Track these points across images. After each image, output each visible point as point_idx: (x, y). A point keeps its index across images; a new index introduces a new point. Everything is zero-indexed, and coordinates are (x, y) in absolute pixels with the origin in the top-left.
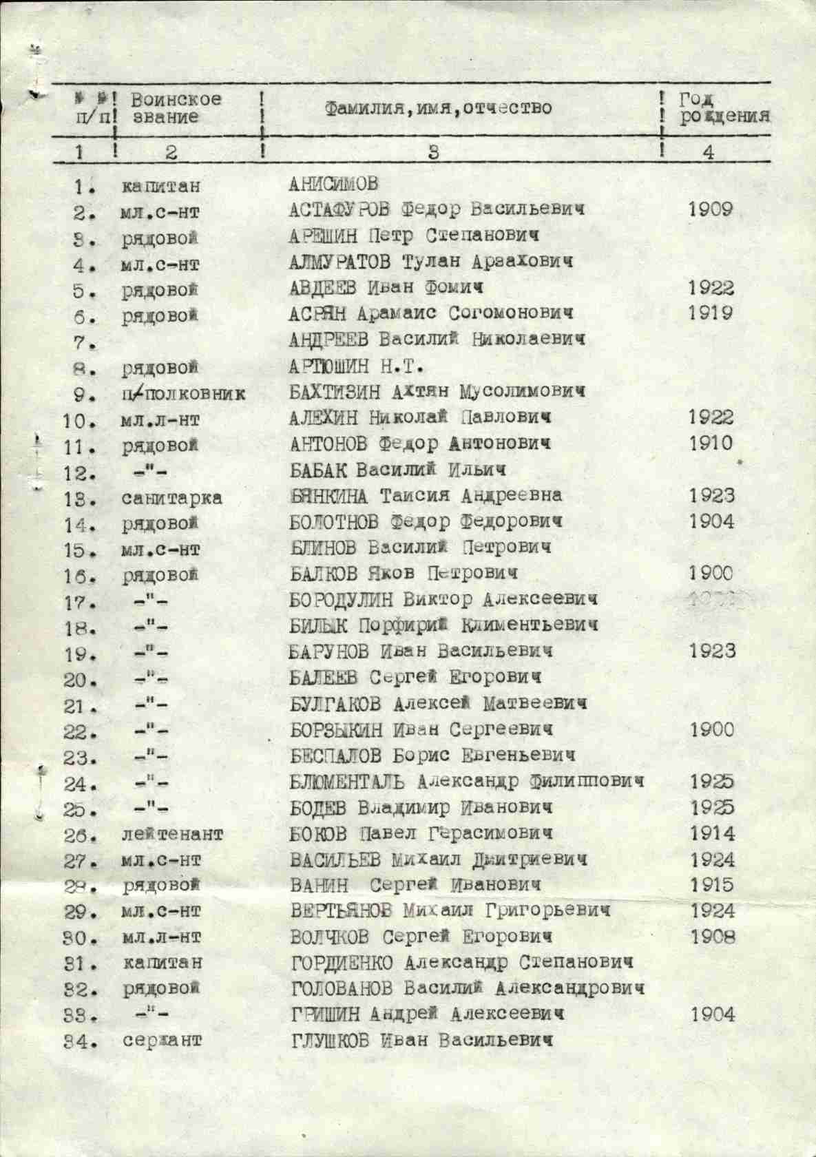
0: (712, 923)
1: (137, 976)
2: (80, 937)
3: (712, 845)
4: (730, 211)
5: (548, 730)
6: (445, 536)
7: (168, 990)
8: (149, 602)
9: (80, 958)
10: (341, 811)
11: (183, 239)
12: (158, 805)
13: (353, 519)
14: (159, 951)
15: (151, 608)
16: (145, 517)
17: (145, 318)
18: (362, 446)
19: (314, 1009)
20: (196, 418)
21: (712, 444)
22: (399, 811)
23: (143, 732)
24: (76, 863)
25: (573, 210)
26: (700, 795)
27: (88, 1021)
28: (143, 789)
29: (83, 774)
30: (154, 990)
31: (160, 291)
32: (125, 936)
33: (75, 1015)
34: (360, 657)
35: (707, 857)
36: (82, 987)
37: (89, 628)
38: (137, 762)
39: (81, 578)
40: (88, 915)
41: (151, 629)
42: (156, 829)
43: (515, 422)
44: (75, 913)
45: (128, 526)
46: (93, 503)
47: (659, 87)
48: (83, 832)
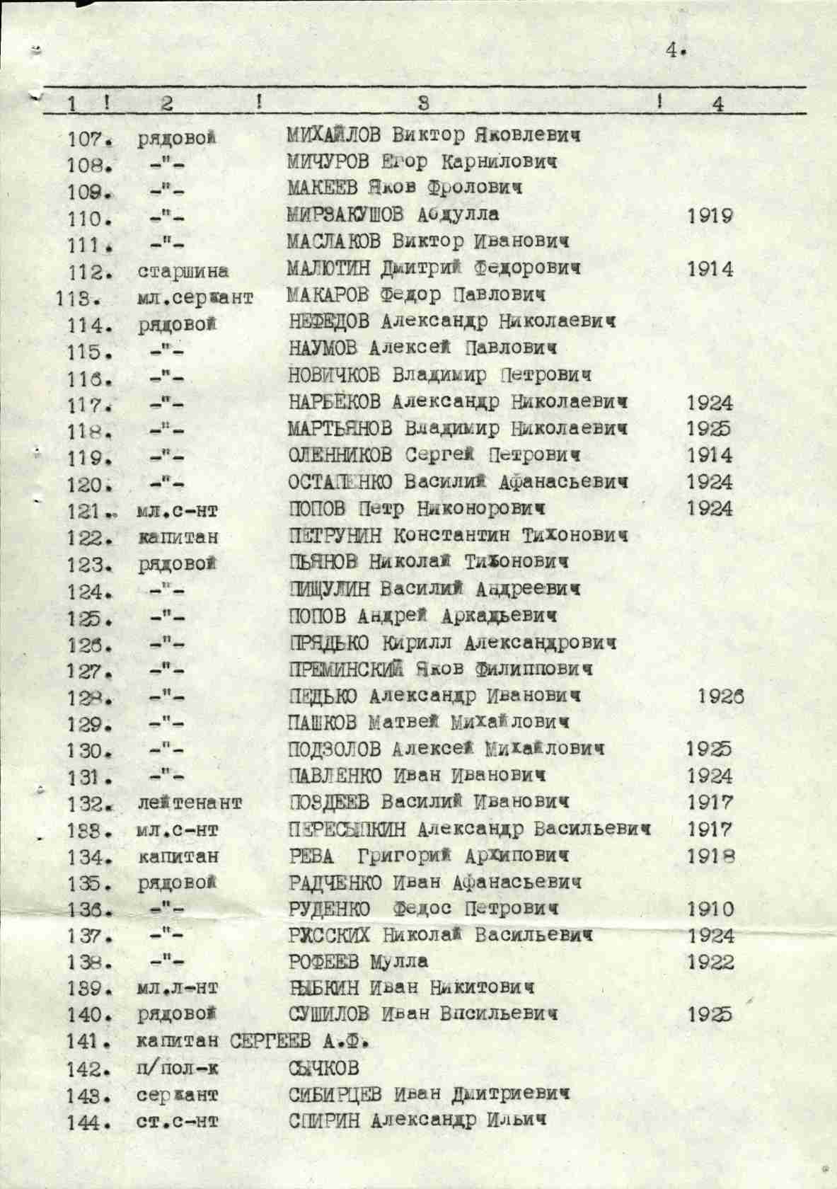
0: (710, 495)
1: (153, 870)
3: (709, 468)
5: (554, 909)
6: (459, 255)
7: (185, 140)
8: (165, 378)
9: (93, 1035)
10: (353, 190)
11: (200, 325)
13: (364, 425)
14: (175, 845)
16: (162, 557)
17: (161, 140)
18: (375, 377)
24: (91, 673)
26: (698, 762)
29: (96, 501)
30: (168, 327)
31: (178, 139)
32: (140, 986)
33: (89, 831)
38: (151, 703)
39: (96, 381)
41: (168, 247)
44: (90, 726)
45: (144, 140)
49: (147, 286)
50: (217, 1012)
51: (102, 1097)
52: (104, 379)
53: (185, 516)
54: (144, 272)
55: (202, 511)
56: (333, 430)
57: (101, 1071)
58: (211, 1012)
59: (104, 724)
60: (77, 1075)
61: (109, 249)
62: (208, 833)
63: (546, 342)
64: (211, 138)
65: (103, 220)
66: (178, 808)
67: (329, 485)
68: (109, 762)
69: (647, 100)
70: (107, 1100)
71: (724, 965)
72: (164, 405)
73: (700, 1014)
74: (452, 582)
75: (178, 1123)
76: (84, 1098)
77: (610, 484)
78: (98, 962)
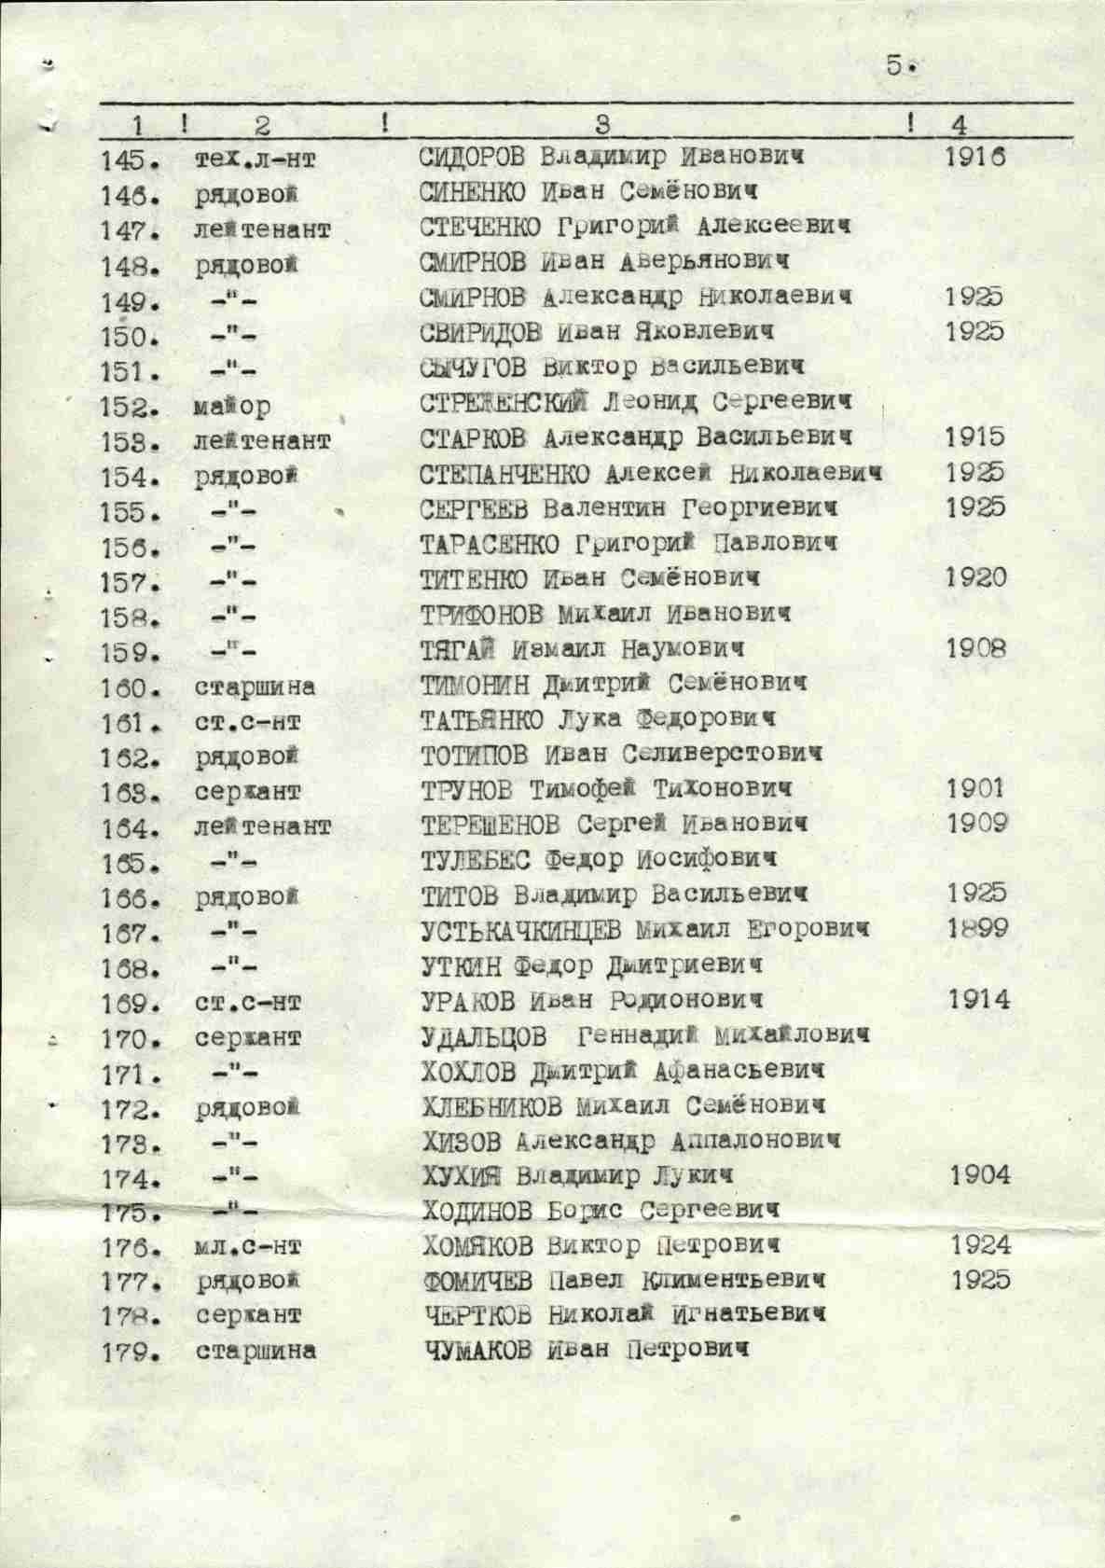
0: (981, 1262)
2: (139, 335)
4: (1005, 930)
8: (231, 371)
9: (137, 715)
12: (244, 1138)
15: (234, 311)
19: (451, 608)
20: (295, 719)
21: (978, 437)
22: (569, 899)
23: (222, 582)
25: (810, 1281)
27: (148, 801)
28: (222, 588)
34: (515, 269)
35: (968, 503)
36: (140, 404)
37: (150, 618)
38: (216, 518)
40: (148, 306)
42: (240, 820)
43: (729, 866)
45: (206, 1283)
46: (155, 307)
47: (909, 109)
48: (140, 190)
49: (210, 705)
50: (299, 895)
51: (149, 794)
52: (150, 547)
53: (259, 1009)
54: (201, 688)
55: (279, 1003)
56: (467, 934)
57: (149, 1112)
58: (291, 755)
59: (150, 1353)
60: (116, 275)
61: (155, 377)
62: (288, 1041)
63: (759, 322)
64: (291, 264)
65: (149, 340)
66: (249, 833)
67: (461, 1007)
68: (157, 1016)
69: (893, 120)
70: (155, 201)
71: (995, 928)
72: (230, 617)
73: (963, 648)
74: (622, 1062)
75: (248, 723)
76: (124, 305)
77: (846, 930)
78: (144, 969)
